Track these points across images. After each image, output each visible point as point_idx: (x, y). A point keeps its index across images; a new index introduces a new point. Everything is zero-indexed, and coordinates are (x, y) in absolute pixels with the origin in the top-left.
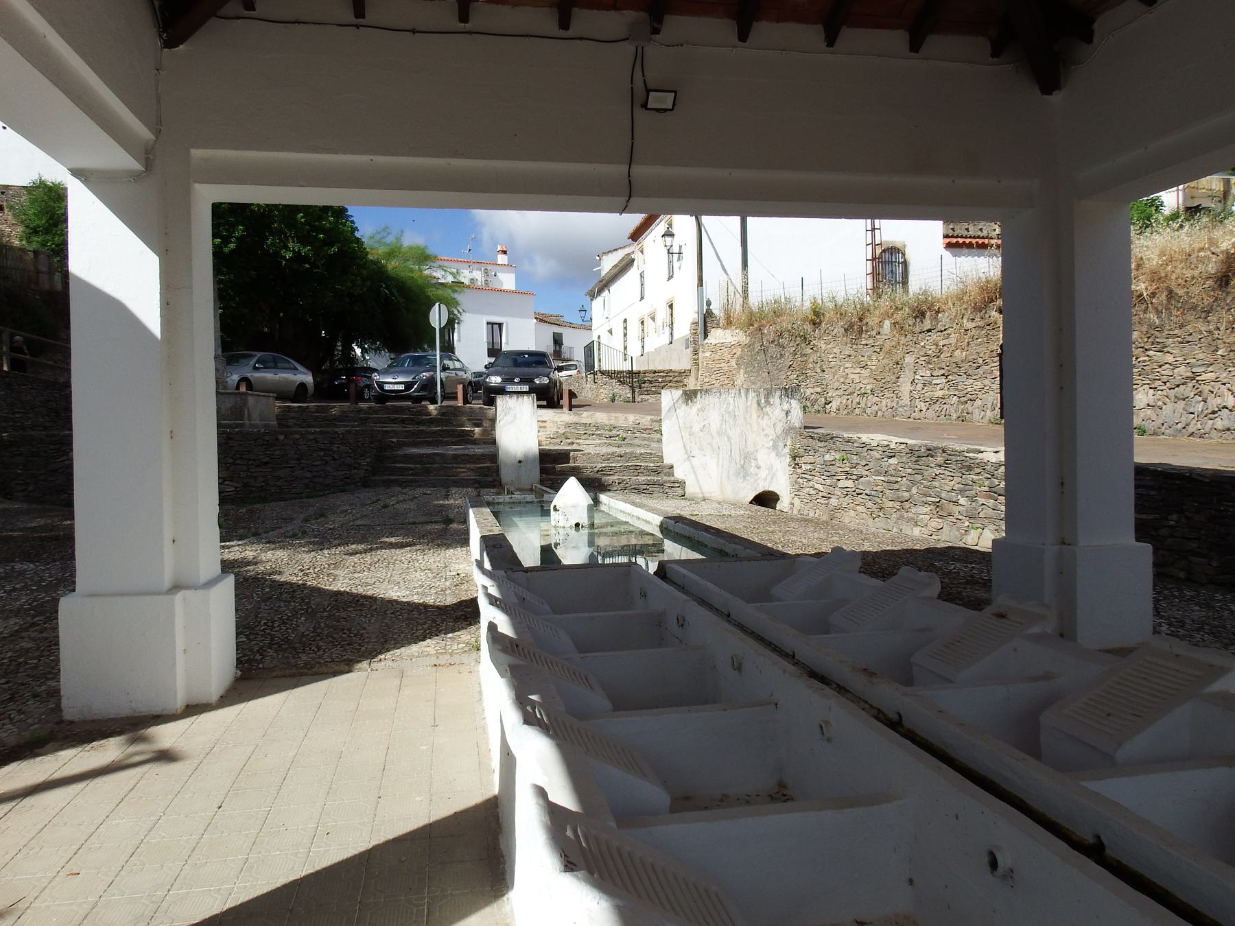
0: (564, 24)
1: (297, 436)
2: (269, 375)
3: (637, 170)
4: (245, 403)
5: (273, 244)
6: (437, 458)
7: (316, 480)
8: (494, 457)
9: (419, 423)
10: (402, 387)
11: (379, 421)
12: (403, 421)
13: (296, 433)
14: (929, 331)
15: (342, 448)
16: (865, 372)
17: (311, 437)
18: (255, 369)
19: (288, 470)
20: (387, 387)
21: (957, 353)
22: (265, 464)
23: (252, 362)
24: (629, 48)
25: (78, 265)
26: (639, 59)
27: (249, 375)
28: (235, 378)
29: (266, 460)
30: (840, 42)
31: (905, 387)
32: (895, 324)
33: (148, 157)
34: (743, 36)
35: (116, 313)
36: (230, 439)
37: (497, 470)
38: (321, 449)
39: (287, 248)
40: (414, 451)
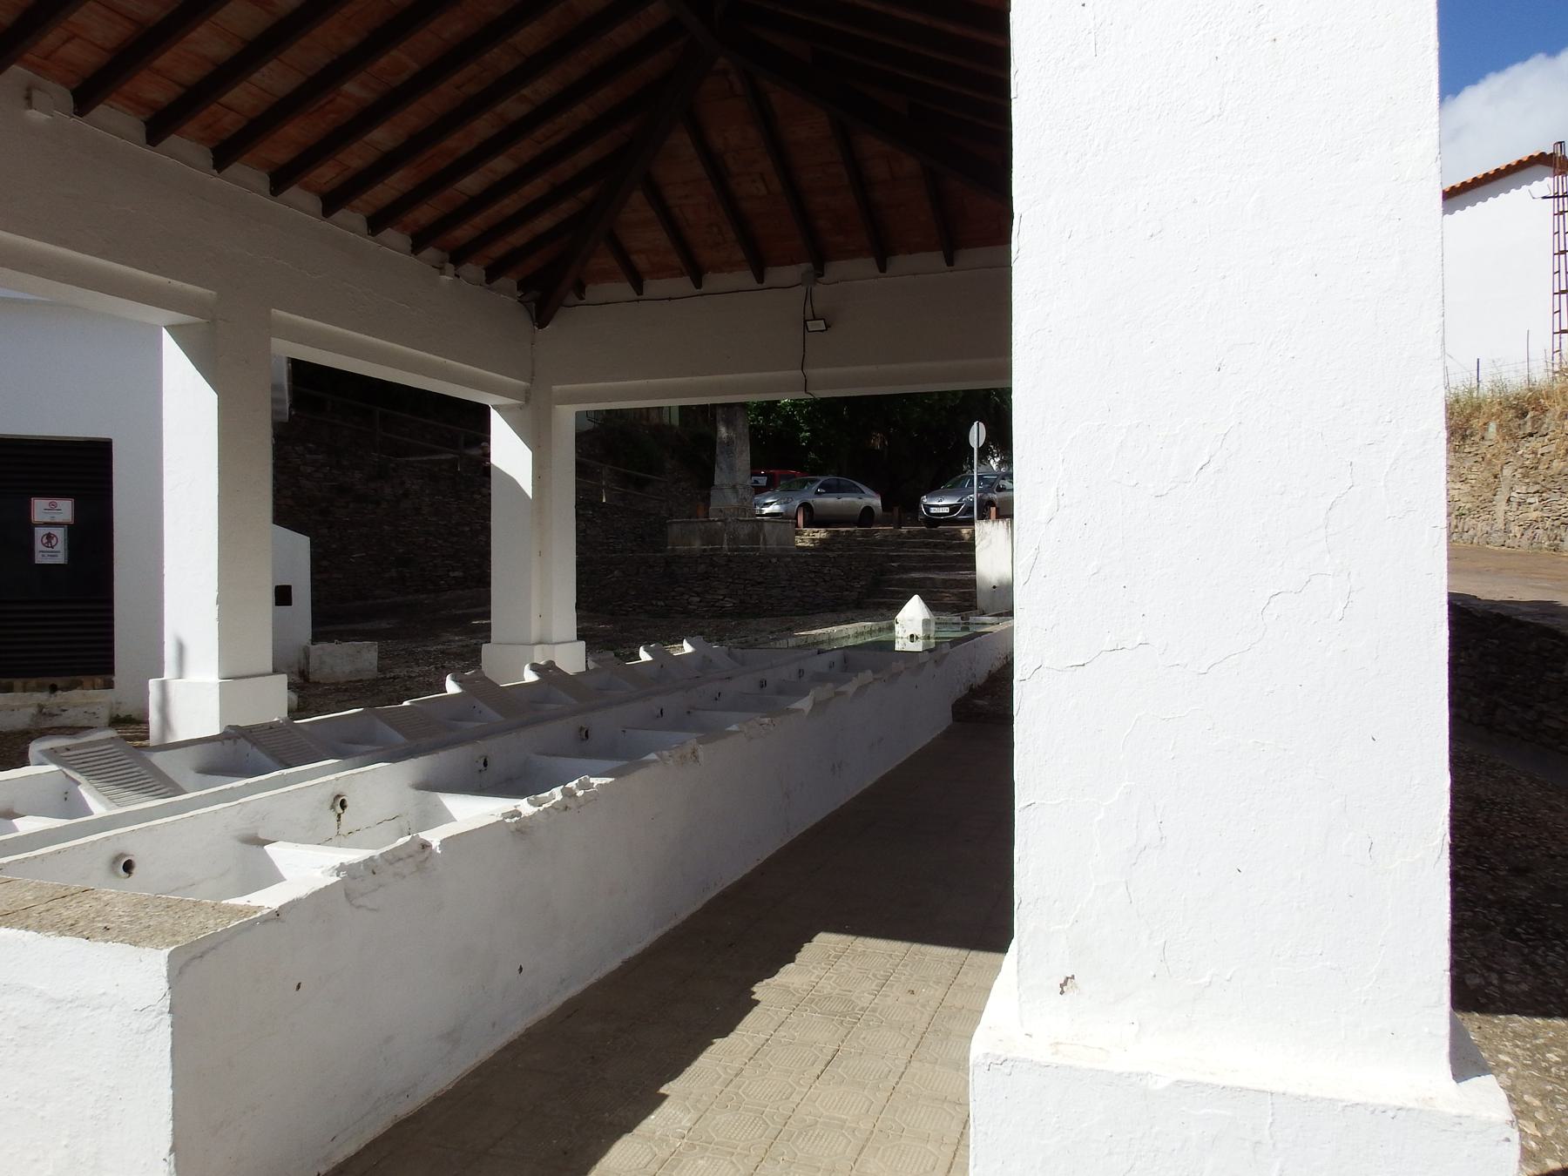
2: (831, 500)
3: (809, 371)
8: (973, 582)
9: (950, 548)
10: (946, 510)
11: (915, 546)
12: (936, 546)
14: (1531, 435)
16: (1466, 488)
20: (933, 510)
21: (1555, 464)
24: (802, 289)
25: (493, 460)
26: (809, 296)
27: (810, 500)
28: (798, 503)
31: (1501, 507)
32: (1500, 426)
33: (527, 397)
34: (883, 269)
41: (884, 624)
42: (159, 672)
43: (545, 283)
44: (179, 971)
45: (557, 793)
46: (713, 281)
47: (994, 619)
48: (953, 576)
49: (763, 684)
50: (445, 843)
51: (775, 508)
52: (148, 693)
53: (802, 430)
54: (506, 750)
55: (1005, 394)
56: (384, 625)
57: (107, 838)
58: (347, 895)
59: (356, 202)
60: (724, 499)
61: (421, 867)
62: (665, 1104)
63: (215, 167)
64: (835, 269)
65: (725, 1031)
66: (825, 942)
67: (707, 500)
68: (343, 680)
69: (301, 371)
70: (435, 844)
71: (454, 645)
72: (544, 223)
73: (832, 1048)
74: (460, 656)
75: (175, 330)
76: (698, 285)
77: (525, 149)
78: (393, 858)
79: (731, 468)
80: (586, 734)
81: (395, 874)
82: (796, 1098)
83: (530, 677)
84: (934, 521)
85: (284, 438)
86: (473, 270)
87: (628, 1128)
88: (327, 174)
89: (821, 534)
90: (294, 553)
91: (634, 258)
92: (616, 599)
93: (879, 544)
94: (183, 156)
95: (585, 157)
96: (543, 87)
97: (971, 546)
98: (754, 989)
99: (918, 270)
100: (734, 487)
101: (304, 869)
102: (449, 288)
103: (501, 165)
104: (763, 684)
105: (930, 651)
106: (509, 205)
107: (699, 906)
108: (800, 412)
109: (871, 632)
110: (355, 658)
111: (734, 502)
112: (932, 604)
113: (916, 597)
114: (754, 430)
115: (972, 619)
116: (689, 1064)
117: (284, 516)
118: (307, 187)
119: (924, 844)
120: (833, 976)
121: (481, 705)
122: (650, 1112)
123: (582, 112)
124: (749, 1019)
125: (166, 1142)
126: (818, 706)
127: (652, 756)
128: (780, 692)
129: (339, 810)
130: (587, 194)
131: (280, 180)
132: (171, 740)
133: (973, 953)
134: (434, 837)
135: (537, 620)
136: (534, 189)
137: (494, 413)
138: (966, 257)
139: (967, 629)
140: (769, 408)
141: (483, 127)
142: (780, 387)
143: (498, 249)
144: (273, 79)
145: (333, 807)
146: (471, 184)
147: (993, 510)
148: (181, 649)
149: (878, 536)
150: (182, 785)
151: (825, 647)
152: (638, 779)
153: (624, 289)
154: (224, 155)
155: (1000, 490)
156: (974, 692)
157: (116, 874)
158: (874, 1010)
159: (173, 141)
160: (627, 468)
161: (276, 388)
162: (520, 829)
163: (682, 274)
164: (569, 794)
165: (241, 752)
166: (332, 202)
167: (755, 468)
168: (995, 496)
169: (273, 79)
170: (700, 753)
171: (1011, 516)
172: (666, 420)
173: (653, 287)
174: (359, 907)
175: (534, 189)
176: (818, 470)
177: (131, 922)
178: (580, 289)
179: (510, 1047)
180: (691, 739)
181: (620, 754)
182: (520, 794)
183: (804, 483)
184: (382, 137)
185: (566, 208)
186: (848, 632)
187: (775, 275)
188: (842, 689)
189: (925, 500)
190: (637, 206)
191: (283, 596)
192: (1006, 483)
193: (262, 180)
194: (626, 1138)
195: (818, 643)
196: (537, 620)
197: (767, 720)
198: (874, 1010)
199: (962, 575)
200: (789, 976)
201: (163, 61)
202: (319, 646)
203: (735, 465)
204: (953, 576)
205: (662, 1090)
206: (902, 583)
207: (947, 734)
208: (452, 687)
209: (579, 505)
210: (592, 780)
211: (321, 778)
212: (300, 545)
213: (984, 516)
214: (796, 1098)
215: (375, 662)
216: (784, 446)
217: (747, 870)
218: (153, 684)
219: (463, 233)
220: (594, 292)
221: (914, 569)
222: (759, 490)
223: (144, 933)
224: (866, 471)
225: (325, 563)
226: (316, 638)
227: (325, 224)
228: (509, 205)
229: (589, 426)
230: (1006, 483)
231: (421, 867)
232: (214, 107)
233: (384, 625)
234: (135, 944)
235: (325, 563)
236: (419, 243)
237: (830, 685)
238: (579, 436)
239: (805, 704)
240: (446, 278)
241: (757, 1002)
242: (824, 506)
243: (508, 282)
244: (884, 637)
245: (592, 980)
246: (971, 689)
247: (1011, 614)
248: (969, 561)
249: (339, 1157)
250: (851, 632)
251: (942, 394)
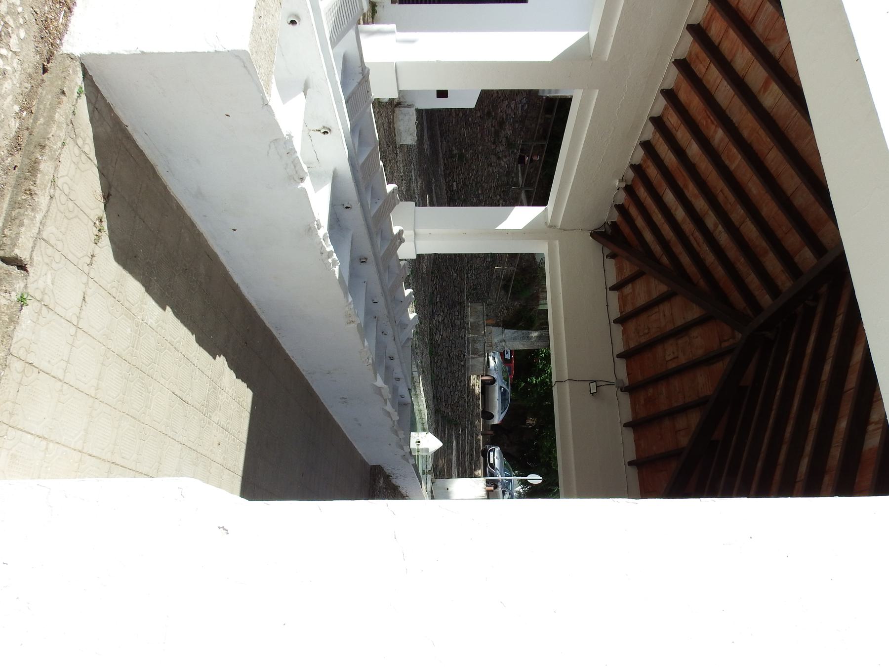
0: (619, 356)
3: (567, 384)
4: (480, 356)
8: (450, 477)
10: (492, 461)
12: (471, 455)
15: (457, 397)
20: (491, 453)
25: (517, 209)
26: (610, 384)
27: (497, 383)
30: (629, 468)
34: (626, 425)
35: (504, 218)
37: (443, 477)
40: (454, 444)
41: (426, 426)
42: (399, 29)
43: (614, 236)
44: (240, 58)
45: (330, 248)
46: (618, 329)
47: (429, 489)
48: (454, 465)
49: (391, 358)
50: (304, 190)
51: (492, 363)
52: (388, 23)
53: (536, 378)
54: (355, 218)
55: (556, 495)
56: (426, 147)
57: (308, 12)
58: (276, 140)
59: (658, 135)
60: (497, 335)
61: (291, 178)
62: (161, 310)
63: (676, 60)
64: (625, 398)
65: (199, 341)
66: (247, 395)
67: (497, 325)
68: (396, 126)
69: (565, 103)
70: (302, 185)
71: (415, 185)
72: (648, 236)
73: (188, 399)
74: (408, 189)
75: (587, 37)
76: (615, 321)
77: (688, 227)
78: (296, 163)
79: (515, 339)
80: (363, 261)
81: (287, 164)
82: (162, 381)
83: (396, 230)
84: (485, 454)
85: (531, 95)
86: (622, 198)
87: (148, 290)
88: (673, 119)
89: (478, 390)
90: (465, 99)
91: (630, 286)
92: (441, 277)
93: (472, 423)
94: (681, 43)
95: (685, 259)
96: (723, 237)
97: (472, 475)
98: (222, 356)
99: (625, 446)
100: (503, 340)
101: (291, 116)
102: (611, 185)
103: (680, 213)
104: (391, 358)
105: (410, 452)
106: (658, 217)
107: (268, 325)
108: (547, 378)
109: (421, 418)
110: (408, 132)
111: (496, 340)
112: (437, 454)
113: (441, 444)
114: (536, 352)
115: (429, 476)
116: (182, 322)
117: (485, 95)
118: (665, 108)
119: (302, 451)
120: (230, 399)
121: (380, 203)
122: (156, 302)
123: (710, 258)
124: (206, 354)
125: (146, 50)
126: (378, 390)
127: (350, 299)
128: (387, 368)
129: (323, 131)
130: (665, 260)
131: (669, 94)
132: (362, 37)
133: (240, 478)
134: (307, 184)
135: (431, 231)
136: (667, 231)
137: (542, 208)
138: (633, 472)
139: (424, 473)
140: (548, 358)
141: (700, 204)
142: (560, 367)
143: (633, 211)
144: (724, 92)
145: (324, 127)
146: (669, 197)
147: (492, 488)
148: (413, 41)
149: (476, 422)
150: (336, 48)
151: (413, 393)
152: (338, 292)
153: (613, 280)
154: (683, 65)
155: (504, 492)
156: (387, 477)
157: (289, 16)
158: (209, 423)
159: (689, 39)
160: (515, 281)
161: (557, 91)
162: (310, 230)
163: (621, 313)
164: (330, 255)
165: (354, 77)
166: (658, 122)
167: (515, 352)
168: (500, 490)
169: (724, 92)
170: (352, 325)
171: (488, 498)
172: (541, 302)
173: (614, 296)
174: (270, 146)
175: (667, 231)
176: (514, 387)
177: (263, 29)
178: (613, 256)
179: (193, 225)
180: (360, 320)
181: (353, 280)
182: (331, 227)
183: (506, 380)
184: (694, 150)
185: (657, 248)
186: (421, 406)
187: (622, 364)
188: (388, 403)
189: (497, 449)
190: (659, 288)
191: (442, 94)
192: (507, 495)
193: (669, 84)
194: (143, 289)
195: (416, 391)
196: (431, 231)
197: (370, 361)
198: (209, 423)
199: (454, 470)
200: (229, 375)
201: (732, 34)
202: (415, 113)
203: (516, 341)
204: (454, 465)
205: (168, 308)
206: (450, 436)
207: (363, 463)
208: (390, 188)
209: (493, 255)
210: (337, 267)
211: (339, 120)
212: (471, 104)
213: (488, 482)
214: (162, 381)
215: (405, 143)
216: (528, 368)
217: (287, 351)
218: (393, 27)
219: (642, 193)
220: (611, 263)
221: (458, 444)
222: (502, 354)
223: (257, 37)
224: (514, 414)
225: (461, 115)
226: (419, 111)
227: (646, 118)
228: (658, 217)
229: (538, 259)
230: (507, 495)
231: (291, 178)
232: (708, 61)
233: (426, 147)
234: (252, 33)
235: (461, 115)
236: (637, 168)
237: (390, 396)
238: (533, 255)
239: (380, 382)
240: (617, 183)
241: (214, 358)
242: (494, 391)
243: (616, 216)
244: (419, 426)
245: (228, 268)
246: (389, 476)
247: (433, 498)
248: (462, 474)
249: (136, 137)
250: (421, 407)
251: (556, 458)
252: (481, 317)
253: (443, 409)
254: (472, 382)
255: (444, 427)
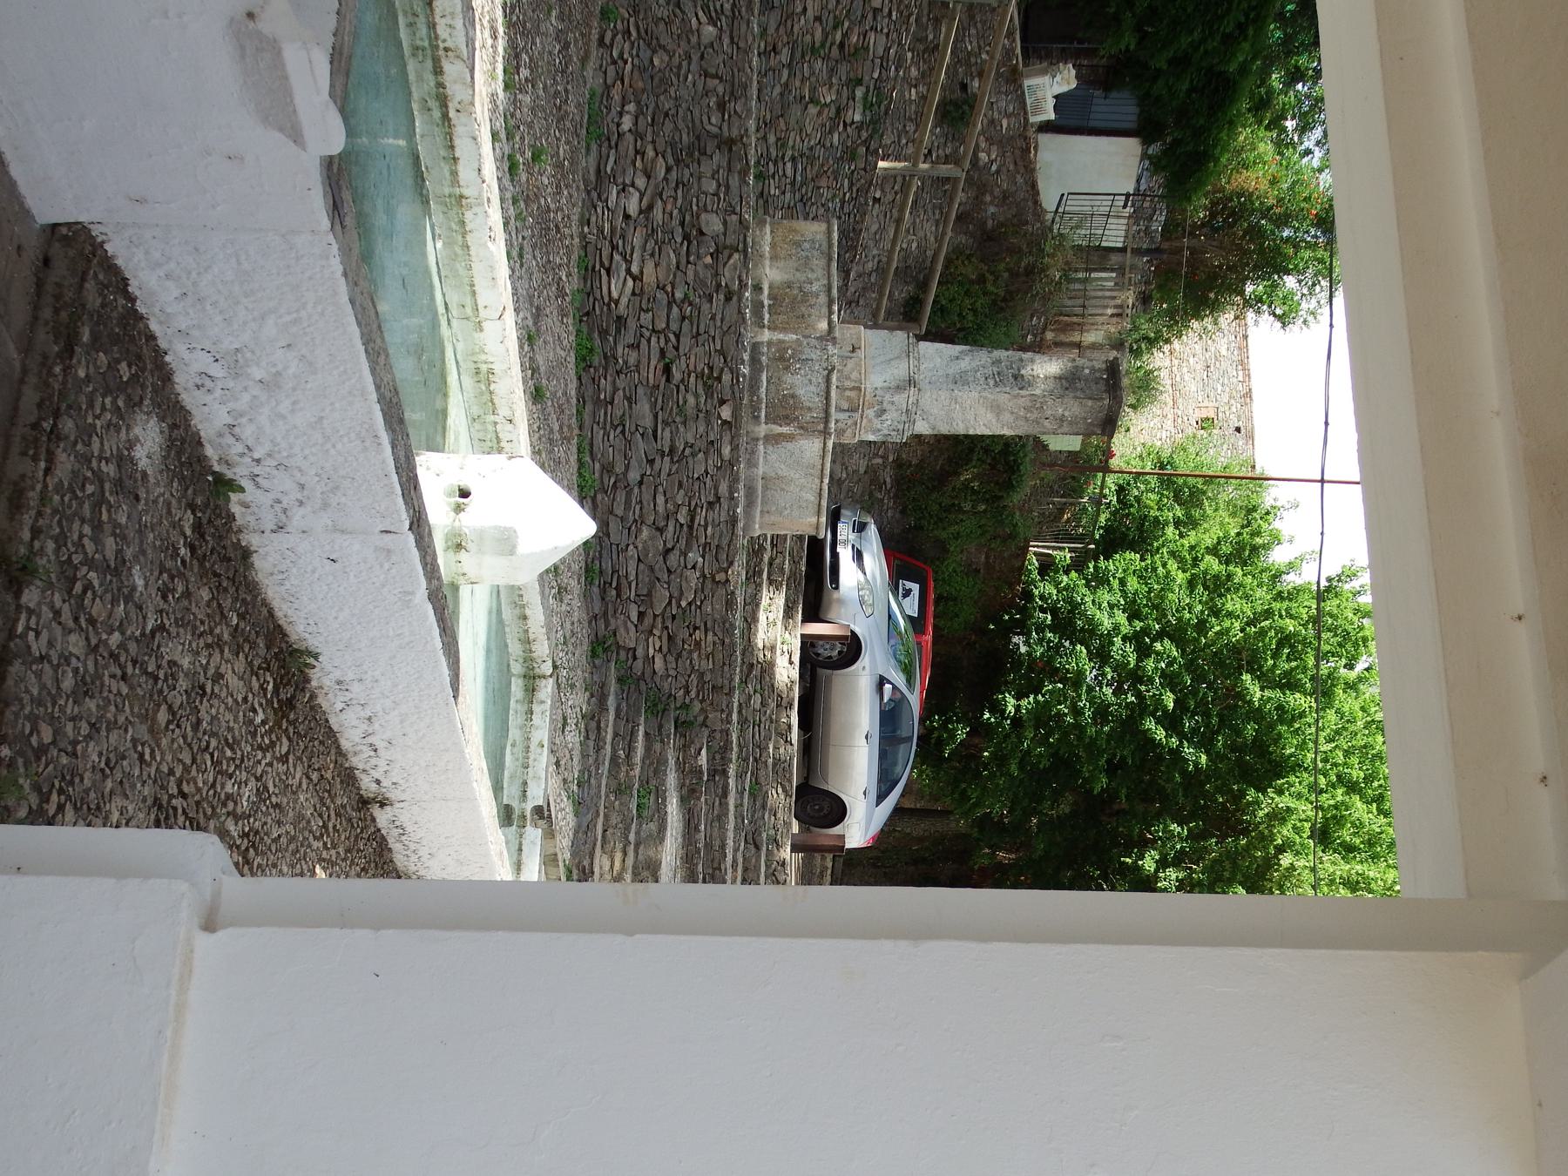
1: (726, 451)
4: (805, 429)
5: (1170, 836)
6: (653, 826)
7: (621, 496)
13: (735, 449)
15: (693, 577)
17: (723, 488)
18: (882, 681)
19: (648, 422)
22: (667, 370)
23: (899, 679)
27: (865, 661)
29: (677, 375)
36: (728, 299)
38: (692, 515)
39: (1162, 864)
79: (960, 380)
89: (786, 672)
100: (911, 382)
108: (1060, 697)
252: (818, 263)
253: (629, 638)
254: (761, 637)
255: (627, 719)
